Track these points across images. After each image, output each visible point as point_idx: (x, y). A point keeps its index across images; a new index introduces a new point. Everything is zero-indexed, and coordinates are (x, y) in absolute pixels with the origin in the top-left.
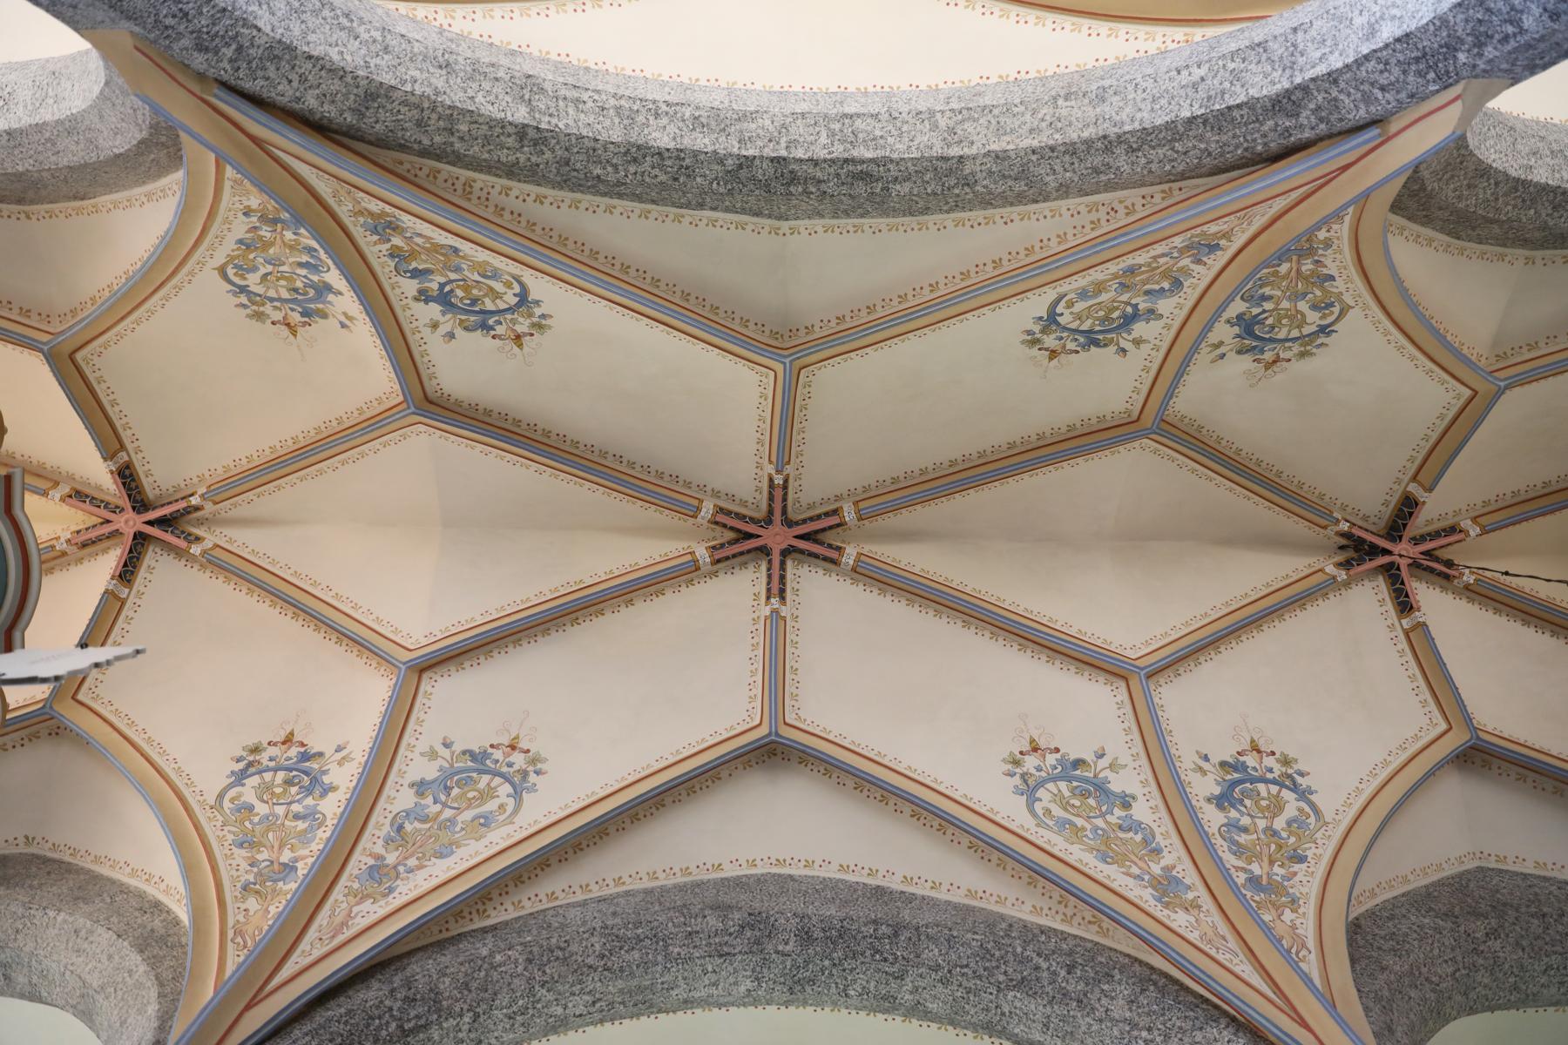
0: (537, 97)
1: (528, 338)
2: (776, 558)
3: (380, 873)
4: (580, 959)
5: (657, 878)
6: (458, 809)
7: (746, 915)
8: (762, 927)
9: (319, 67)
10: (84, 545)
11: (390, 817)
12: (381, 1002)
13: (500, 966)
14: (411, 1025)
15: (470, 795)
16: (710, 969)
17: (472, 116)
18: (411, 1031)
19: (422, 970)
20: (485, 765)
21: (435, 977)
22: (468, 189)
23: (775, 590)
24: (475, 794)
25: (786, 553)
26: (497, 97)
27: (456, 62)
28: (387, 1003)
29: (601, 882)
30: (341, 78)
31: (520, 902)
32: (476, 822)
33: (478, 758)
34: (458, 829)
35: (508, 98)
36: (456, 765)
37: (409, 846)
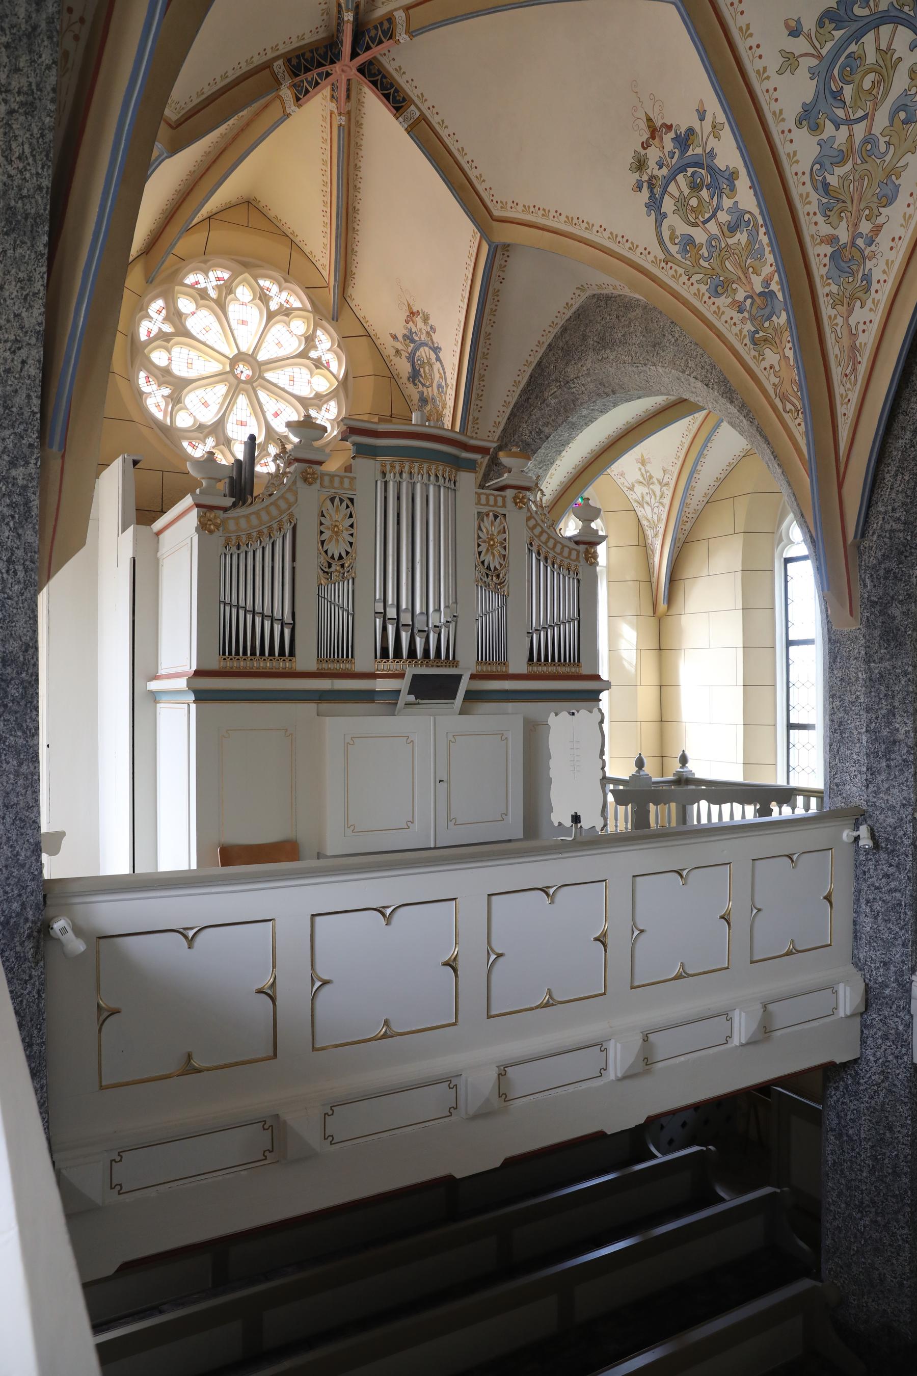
6: (865, 117)
10: (348, 97)
11: (807, 178)
15: (867, 84)
24: (871, 77)
32: (897, 123)
34: (883, 148)
36: (824, 52)
37: (849, 204)
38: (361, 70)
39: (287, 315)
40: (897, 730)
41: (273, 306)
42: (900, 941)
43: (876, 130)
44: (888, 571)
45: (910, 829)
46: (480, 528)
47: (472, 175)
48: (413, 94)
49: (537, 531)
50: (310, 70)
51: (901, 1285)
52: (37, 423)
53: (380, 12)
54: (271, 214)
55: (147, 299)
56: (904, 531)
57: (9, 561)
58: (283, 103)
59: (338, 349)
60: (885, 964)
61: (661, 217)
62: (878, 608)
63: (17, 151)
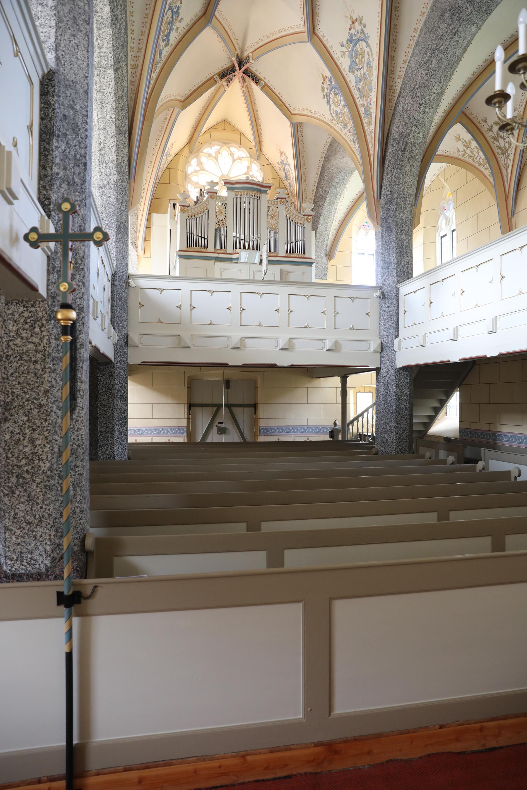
0: (102, 65)
3: (367, 110)
4: (423, 82)
5: (424, 13)
7: (449, 13)
8: (456, 11)
9: (118, 155)
12: (393, 151)
13: (407, 108)
14: (403, 148)
16: (457, 39)
17: (116, 91)
18: (405, 148)
19: (394, 133)
21: (397, 130)
22: (134, 67)
26: (107, 82)
27: (99, 99)
28: (394, 149)
29: (411, 38)
30: (118, 145)
31: (399, 76)
35: (106, 77)
36: (350, 50)
38: (244, 73)
39: (240, 160)
40: (391, 259)
41: (236, 157)
42: (392, 328)
43: (365, 71)
44: (387, 208)
45: (395, 291)
46: (268, 211)
47: (284, 100)
48: (262, 77)
49: (289, 211)
50: (226, 76)
51: (392, 442)
52: (128, 174)
53: (245, 55)
54: (233, 124)
55: (190, 158)
56: (390, 194)
57: (122, 202)
58: (224, 86)
59: (260, 171)
60: (388, 336)
61: (330, 105)
62: (385, 220)
63: (120, 118)
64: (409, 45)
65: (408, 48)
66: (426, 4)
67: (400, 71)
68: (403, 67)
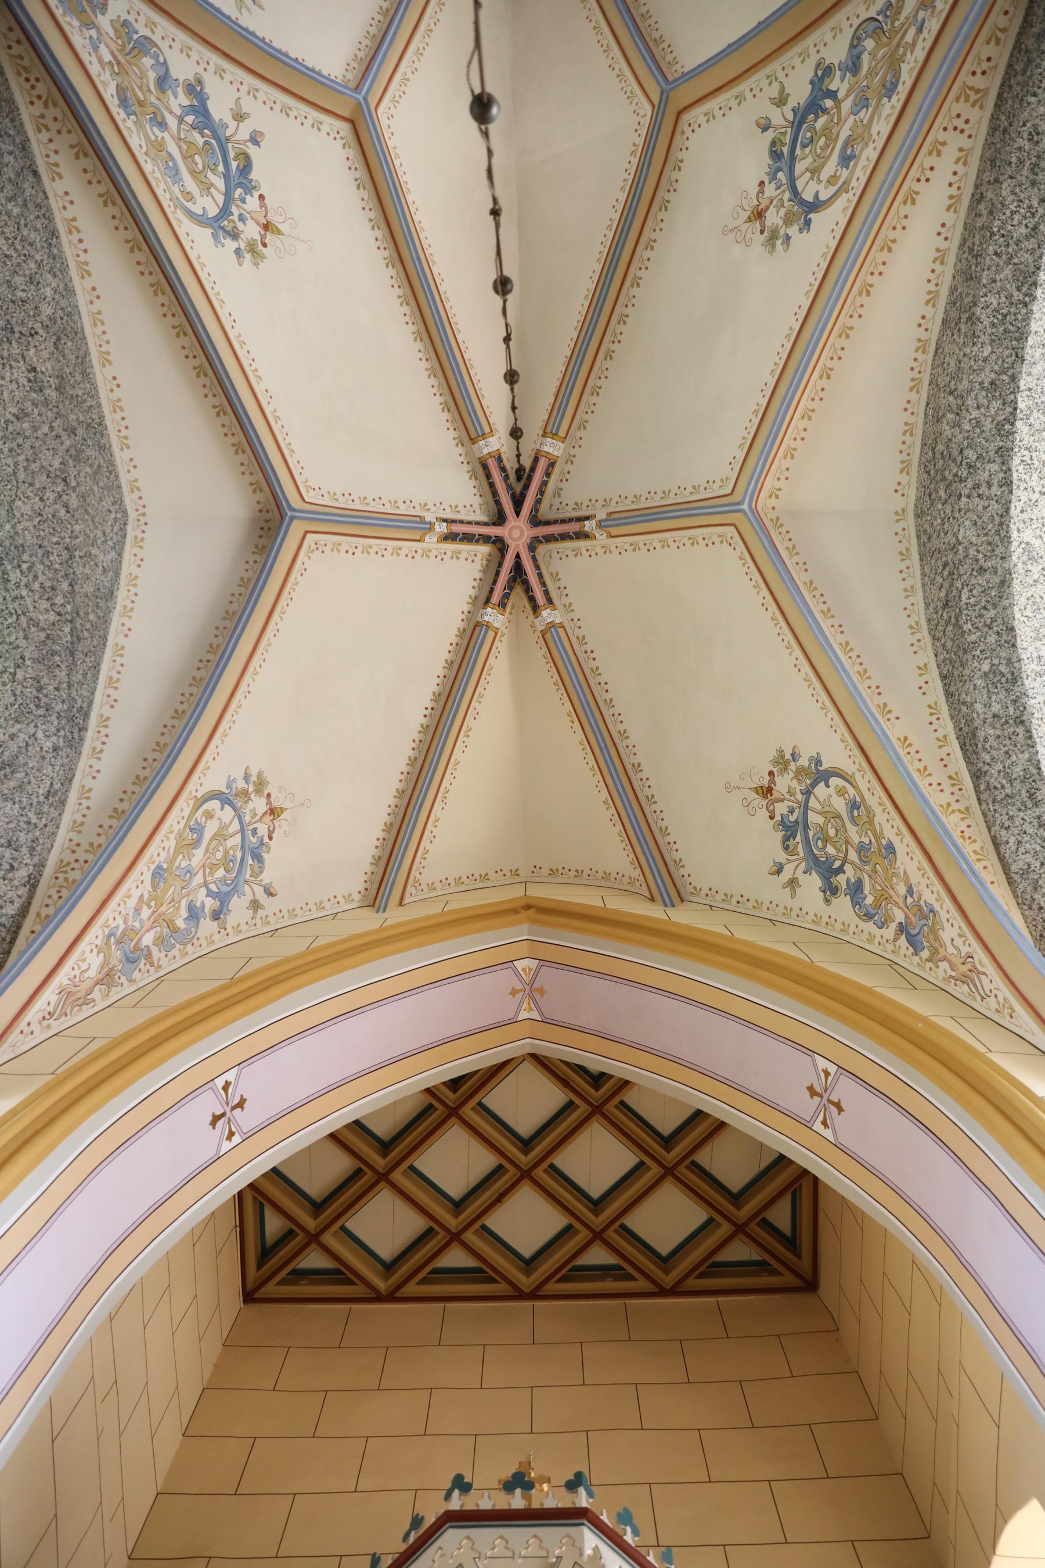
1: (759, 228)
2: (493, 531)
20: (797, 822)
23: (457, 528)
25: (500, 545)
33: (789, 830)
64: (810, 418)
65: (813, 411)
66: (589, 412)
67: (788, 469)
68: (65, 208)
